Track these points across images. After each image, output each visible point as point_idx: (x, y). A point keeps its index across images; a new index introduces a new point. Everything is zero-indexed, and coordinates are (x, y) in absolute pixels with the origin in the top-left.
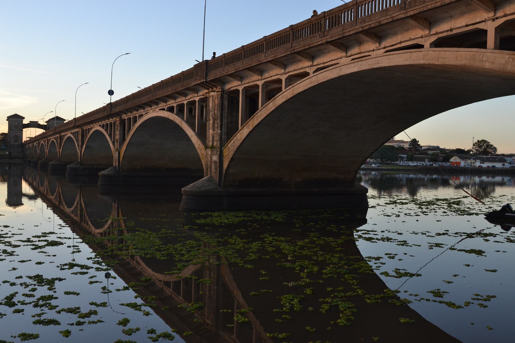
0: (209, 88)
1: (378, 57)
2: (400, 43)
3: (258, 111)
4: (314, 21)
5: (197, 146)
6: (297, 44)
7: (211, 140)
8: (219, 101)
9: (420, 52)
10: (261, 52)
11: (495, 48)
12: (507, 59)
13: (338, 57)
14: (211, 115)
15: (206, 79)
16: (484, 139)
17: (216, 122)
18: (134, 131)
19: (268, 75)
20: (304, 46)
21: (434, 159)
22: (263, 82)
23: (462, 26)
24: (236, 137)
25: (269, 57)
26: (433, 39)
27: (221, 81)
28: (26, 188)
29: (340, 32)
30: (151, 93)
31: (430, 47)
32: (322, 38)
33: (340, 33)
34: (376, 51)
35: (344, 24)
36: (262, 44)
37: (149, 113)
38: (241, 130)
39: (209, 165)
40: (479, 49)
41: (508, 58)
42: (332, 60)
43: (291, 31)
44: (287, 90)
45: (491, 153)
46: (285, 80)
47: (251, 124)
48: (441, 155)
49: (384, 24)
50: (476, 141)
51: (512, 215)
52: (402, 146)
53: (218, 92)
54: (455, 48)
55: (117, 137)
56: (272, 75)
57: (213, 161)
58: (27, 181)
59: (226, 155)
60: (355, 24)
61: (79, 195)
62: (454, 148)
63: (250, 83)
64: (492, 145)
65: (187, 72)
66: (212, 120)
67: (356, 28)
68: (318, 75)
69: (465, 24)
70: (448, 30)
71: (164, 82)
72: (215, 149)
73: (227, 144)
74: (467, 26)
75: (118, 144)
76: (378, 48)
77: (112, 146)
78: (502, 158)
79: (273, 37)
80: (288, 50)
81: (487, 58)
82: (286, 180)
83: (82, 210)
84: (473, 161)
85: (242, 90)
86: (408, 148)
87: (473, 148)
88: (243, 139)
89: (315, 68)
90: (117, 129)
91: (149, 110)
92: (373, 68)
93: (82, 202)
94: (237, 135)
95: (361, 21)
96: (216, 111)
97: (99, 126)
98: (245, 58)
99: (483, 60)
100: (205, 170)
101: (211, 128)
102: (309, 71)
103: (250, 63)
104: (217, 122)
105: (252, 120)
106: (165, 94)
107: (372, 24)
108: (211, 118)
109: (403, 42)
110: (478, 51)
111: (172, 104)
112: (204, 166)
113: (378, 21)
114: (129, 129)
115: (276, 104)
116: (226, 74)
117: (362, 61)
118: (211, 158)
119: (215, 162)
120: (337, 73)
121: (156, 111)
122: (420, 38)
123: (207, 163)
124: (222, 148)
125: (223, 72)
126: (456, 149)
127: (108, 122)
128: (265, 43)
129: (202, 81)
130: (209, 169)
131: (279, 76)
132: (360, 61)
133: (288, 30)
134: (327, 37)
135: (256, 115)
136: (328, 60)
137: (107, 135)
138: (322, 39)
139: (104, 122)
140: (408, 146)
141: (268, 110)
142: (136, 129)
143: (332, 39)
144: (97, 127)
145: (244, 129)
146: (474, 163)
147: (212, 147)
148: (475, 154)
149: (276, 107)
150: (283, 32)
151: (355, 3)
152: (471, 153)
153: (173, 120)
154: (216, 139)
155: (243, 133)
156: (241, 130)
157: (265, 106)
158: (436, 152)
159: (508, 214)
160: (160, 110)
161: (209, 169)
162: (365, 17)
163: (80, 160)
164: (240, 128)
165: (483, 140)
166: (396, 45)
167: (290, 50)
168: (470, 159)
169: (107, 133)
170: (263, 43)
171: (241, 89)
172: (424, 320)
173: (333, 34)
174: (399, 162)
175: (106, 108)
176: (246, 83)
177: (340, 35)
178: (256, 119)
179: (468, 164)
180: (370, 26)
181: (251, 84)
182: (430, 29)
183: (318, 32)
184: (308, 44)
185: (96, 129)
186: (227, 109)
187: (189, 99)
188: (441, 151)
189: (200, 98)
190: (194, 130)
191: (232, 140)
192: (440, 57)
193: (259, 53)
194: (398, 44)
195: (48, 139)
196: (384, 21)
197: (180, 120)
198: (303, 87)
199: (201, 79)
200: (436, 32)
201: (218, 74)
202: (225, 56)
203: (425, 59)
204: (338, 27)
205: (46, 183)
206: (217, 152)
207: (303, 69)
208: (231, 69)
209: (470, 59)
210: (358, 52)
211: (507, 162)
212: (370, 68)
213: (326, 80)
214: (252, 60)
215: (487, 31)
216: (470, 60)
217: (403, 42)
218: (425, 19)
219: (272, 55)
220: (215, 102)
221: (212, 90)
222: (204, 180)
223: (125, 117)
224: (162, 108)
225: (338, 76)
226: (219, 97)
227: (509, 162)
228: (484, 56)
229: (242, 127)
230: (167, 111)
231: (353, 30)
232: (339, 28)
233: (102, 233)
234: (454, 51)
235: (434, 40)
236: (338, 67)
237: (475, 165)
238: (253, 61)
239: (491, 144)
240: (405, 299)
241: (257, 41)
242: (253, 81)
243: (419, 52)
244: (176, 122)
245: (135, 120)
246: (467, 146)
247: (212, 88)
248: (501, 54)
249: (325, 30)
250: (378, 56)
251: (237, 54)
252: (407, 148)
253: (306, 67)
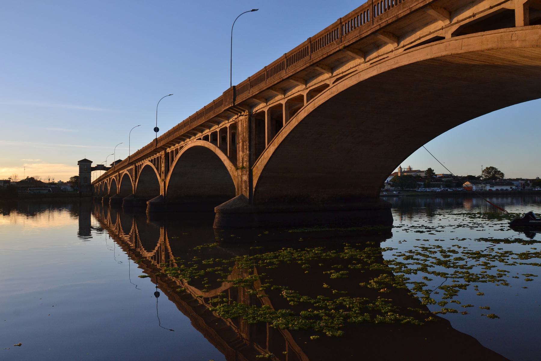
0: (237, 113)
1: (397, 57)
2: (420, 39)
3: (283, 128)
4: (331, 29)
5: (229, 169)
6: (316, 55)
9: (442, 43)
11: (525, 24)
13: (357, 64)
14: (240, 138)
15: (234, 104)
16: (492, 166)
17: (245, 144)
20: (322, 55)
24: (263, 156)
26: (455, 28)
27: (248, 105)
28: (94, 222)
29: (357, 34)
32: (340, 44)
34: (395, 51)
36: (283, 61)
38: (268, 148)
39: (240, 185)
40: (507, 29)
42: (351, 68)
43: (310, 44)
45: (499, 178)
48: (455, 181)
49: (401, 17)
50: (484, 168)
51: (536, 221)
52: (419, 175)
53: (245, 115)
54: (480, 33)
55: (163, 169)
58: (93, 214)
61: (133, 225)
62: (465, 175)
64: (500, 171)
65: (217, 100)
66: (242, 142)
67: (373, 27)
69: (489, 7)
74: (491, 8)
75: (164, 175)
76: (396, 48)
77: (159, 177)
78: (510, 182)
79: (293, 53)
80: (307, 63)
81: (517, 37)
82: (314, 197)
84: (483, 185)
86: (425, 176)
87: (482, 174)
88: (270, 157)
89: (334, 79)
90: (163, 162)
93: (168, 244)
94: (264, 154)
95: (378, 20)
100: (236, 190)
101: (241, 150)
104: (246, 143)
108: (240, 141)
109: (422, 37)
110: (506, 31)
111: (207, 133)
112: (236, 187)
113: (396, 15)
114: (173, 160)
115: (299, 119)
116: (252, 96)
117: (381, 63)
118: (242, 178)
119: (245, 181)
120: (356, 80)
122: (440, 29)
124: (251, 168)
125: (249, 95)
126: (468, 176)
129: (231, 106)
131: (301, 92)
132: (378, 64)
134: (345, 42)
135: (281, 132)
136: (347, 69)
137: (155, 169)
140: (425, 175)
143: (349, 43)
144: (147, 162)
145: (270, 148)
146: (485, 187)
147: (243, 168)
148: (485, 180)
149: (299, 122)
150: (301, 46)
151: (371, 2)
152: (481, 178)
153: (208, 147)
155: (270, 151)
156: (268, 148)
158: (450, 179)
159: (532, 221)
160: (197, 140)
162: (382, 15)
163: (134, 193)
165: (491, 167)
168: (480, 183)
171: (266, 110)
174: (417, 189)
176: (271, 104)
177: (357, 38)
178: (281, 136)
179: (480, 188)
180: (388, 22)
182: (451, 19)
184: (326, 52)
186: (254, 131)
190: (226, 154)
192: (463, 44)
193: (281, 71)
194: (417, 40)
195: (110, 177)
196: (401, 14)
198: (324, 99)
200: (458, 20)
201: (245, 97)
202: (250, 79)
203: (447, 50)
204: (355, 30)
205: (118, 220)
211: (514, 185)
212: (389, 69)
213: (345, 88)
214: (274, 78)
216: (498, 42)
217: (422, 37)
218: (445, 9)
219: (292, 70)
224: (198, 138)
225: (357, 82)
227: (515, 185)
228: (513, 35)
229: (269, 145)
231: (370, 30)
233: (153, 257)
234: (478, 36)
235: (455, 30)
237: (485, 189)
239: (498, 170)
241: (278, 59)
242: (277, 101)
243: (440, 43)
244: (211, 149)
245: (177, 151)
246: (477, 172)
247: (241, 113)
248: (532, 29)
249: (342, 36)
250: (397, 56)
252: (423, 176)
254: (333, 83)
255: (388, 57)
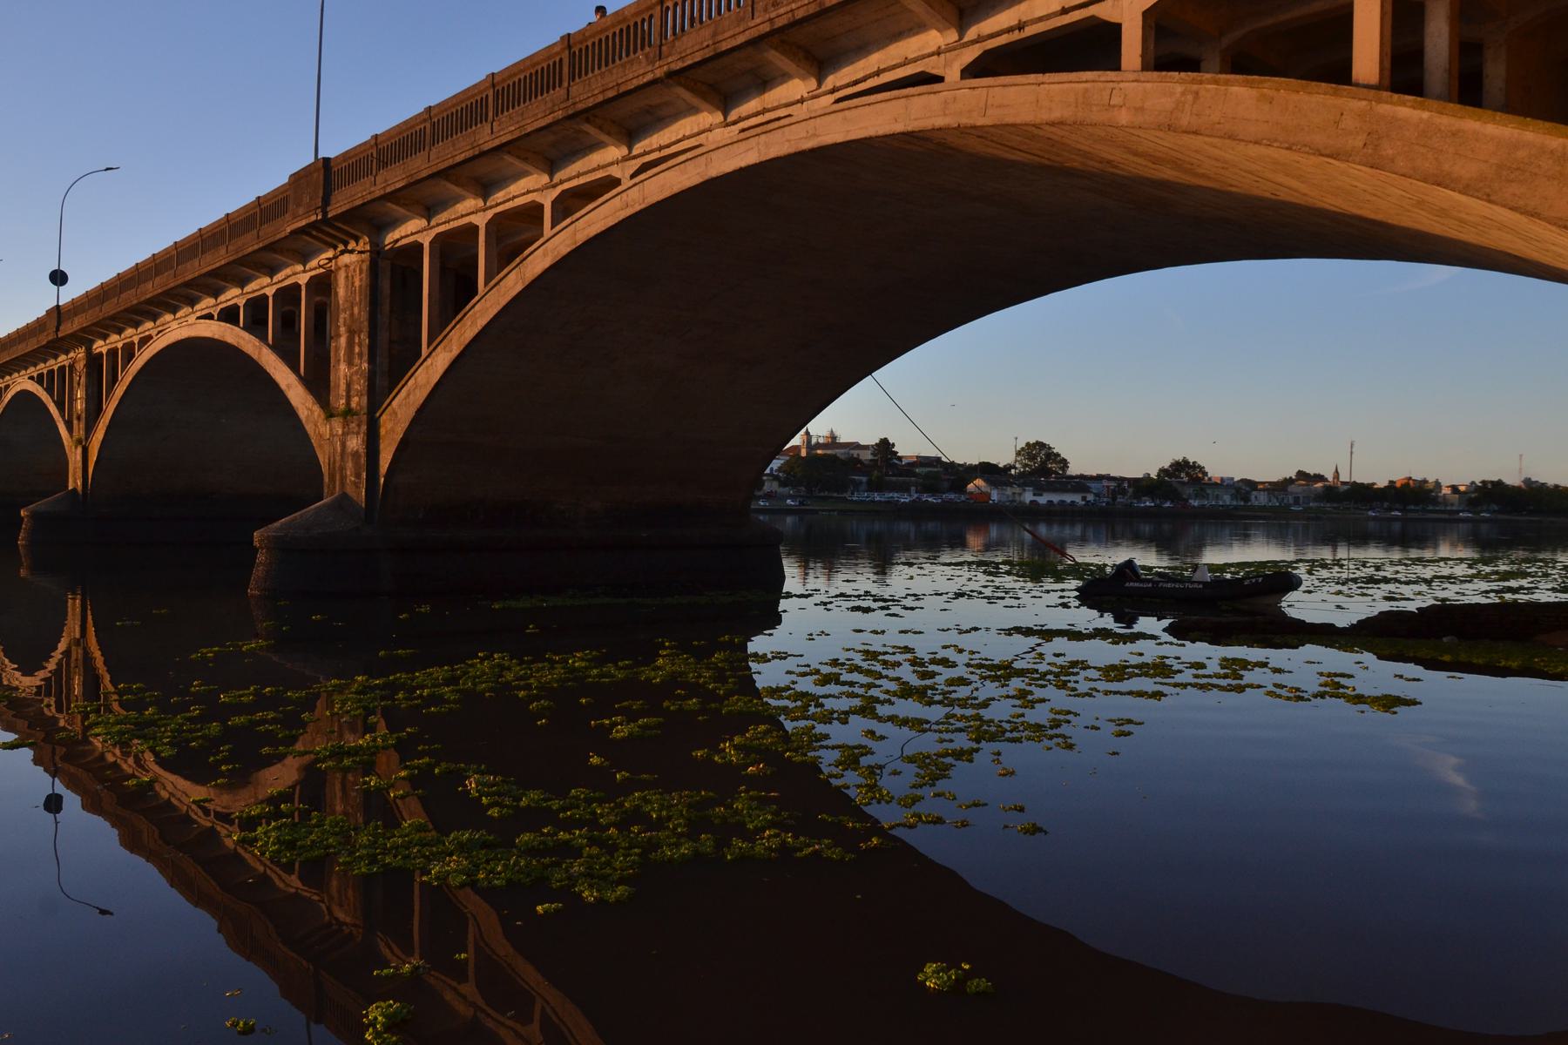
0: (335, 242)
1: (815, 117)
2: (878, 73)
3: (477, 298)
5: (303, 414)
7: (344, 394)
8: (364, 279)
10: (481, 122)
11: (1145, 68)
12: (1178, 95)
13: (702, 128)
14: (341, 320)
15: (325, 213)
18: (128, 384)
19: (504, 196)
21: (930, 486)
22: (490, 217)
23: (1050, 11)
24: (413, 378)
25: (502, 133)
30: (172, 268)
31: (962, 78)
33: (705, 44)
34: (809, 102)
35: (719, 18)
37: (167, 330)
39: (337, 465)
41: (1183, 94)
42: (685, 138)
44: (557, 233)
46: (550, 204)
47: (455, 338)
50: (1021, 444)
51: (1141, 585)
52: (855, 456)
55: (80, 406)
56: (515, 194)
57: (350, 450)
59: (386, 432)
60: (751, 14)
62: (974, 460)
63: (451, 223)
64: (1058, 455)
68: (645, 182)
69: (1059, 8)
70: (1012, 27)
71: (208, 232)
72: (355, 417)
73: (388, 401)
75: (82, 425)
78: (1081, 483)
79: (515, 75)
80: (556, 108)
81: (1122, 97)
83: (92, 682)
84: (1018, 490)
85: (430, 242)
86: (871, 460)
87: (1016, 461)
89: (635, 164)
90: (79, 384)
91: (168, 322)
92: (800, 149)
96: (356, 310)
97: (29, 378)
98: (434, 144)
99: (1111, 103)
100: (326, 479)
102: (618, 175)
103: (449, 156)
104: (360, 337)
105: (458, 326)
106: (210, 268)
107: (798, 8)
108: (342, 329)
109: (885, 70)
111: (233, 298)
112: (325, 469)
114: (114, 380)
116: (382, 192)
117: (770, 131)
118: (344, 445)
119: (356, 454)
120: (698, 174)
121: (189, 323)
122: (932, 54)
123: (332, 459)
124: (375, 413)
125: (372, 189)
127: (53, 364)
128: (491, 93)
129: (313, 218)
130: (338, 478)
131: (535, 194)
133: (557, 49)
134: (670, 60)
136: (673, 139)
137: (52, 404)
138: (653, 66)
139: (42, 368)
140: (870, 457)
141: (504, 294)
142: (131, 379)
143: (683, 62)
146: (1020, 494)
147: (348, 412)
148: (1021, 475)
152: (1013, 471)
154: (357, 389)
157: (495, 286)
158: (936, 470)
159: (1132, 584)
161: (338, 478)
164: (425, 351)
165: (1038, 443)
166: (865, 81)
167: (562, 106)
168: (1011, 485)
169: (52, 397)
170: (487, 96)
171: (426, 240)
172: (932, 862)
173: (685, 50)
175: (45, 323)
177: (706, 50)
180: (793, 16)
181: (456, 226)
183: (642, 49)
184: (615, 84)
185: (19, 390)
186: (388, 301)
187: (279, 282)
188: (946, 469)
189: (311, 277)
190: (294, 368)
191: (403, 386)
193: (476, 125)
194: (870, 77)
197: (256, 342)
199: (310, 213)
201: (360, 195)
202: (379, 141)
204: (701, 28)
206: (359, 426)
207: (601, 171)
208: (394, 178)
209: (1077, 103)
210: (759, 109)
211: (1091, 492)
212: (792, 150)
213: (667, 194)
215: (1119, 26)
217: (885, 70)
220: (353, 283)
221: (343, 248)
222: (324, 505)
223: (100, 346)
224: (204, 312)
225: (701, 180)
226: (365, 267)
229: (431, 348)
230: (219, 320)
231: (744, 31)
232: (703, 30)
236: (703, 154)
238: (456, 150)
239: (1055, 451)
240: (1051, 641)
242: (462, 216)
243: (931, 93)
244: (245, 349)
245: (129, 352)
246: (1003, 456)
247: (346, 244)
248: (1161, 82)
249: (664, 41)
251: (412, 134)
253: (612, 164)
254: (632, 177)
255: (700, 145)
